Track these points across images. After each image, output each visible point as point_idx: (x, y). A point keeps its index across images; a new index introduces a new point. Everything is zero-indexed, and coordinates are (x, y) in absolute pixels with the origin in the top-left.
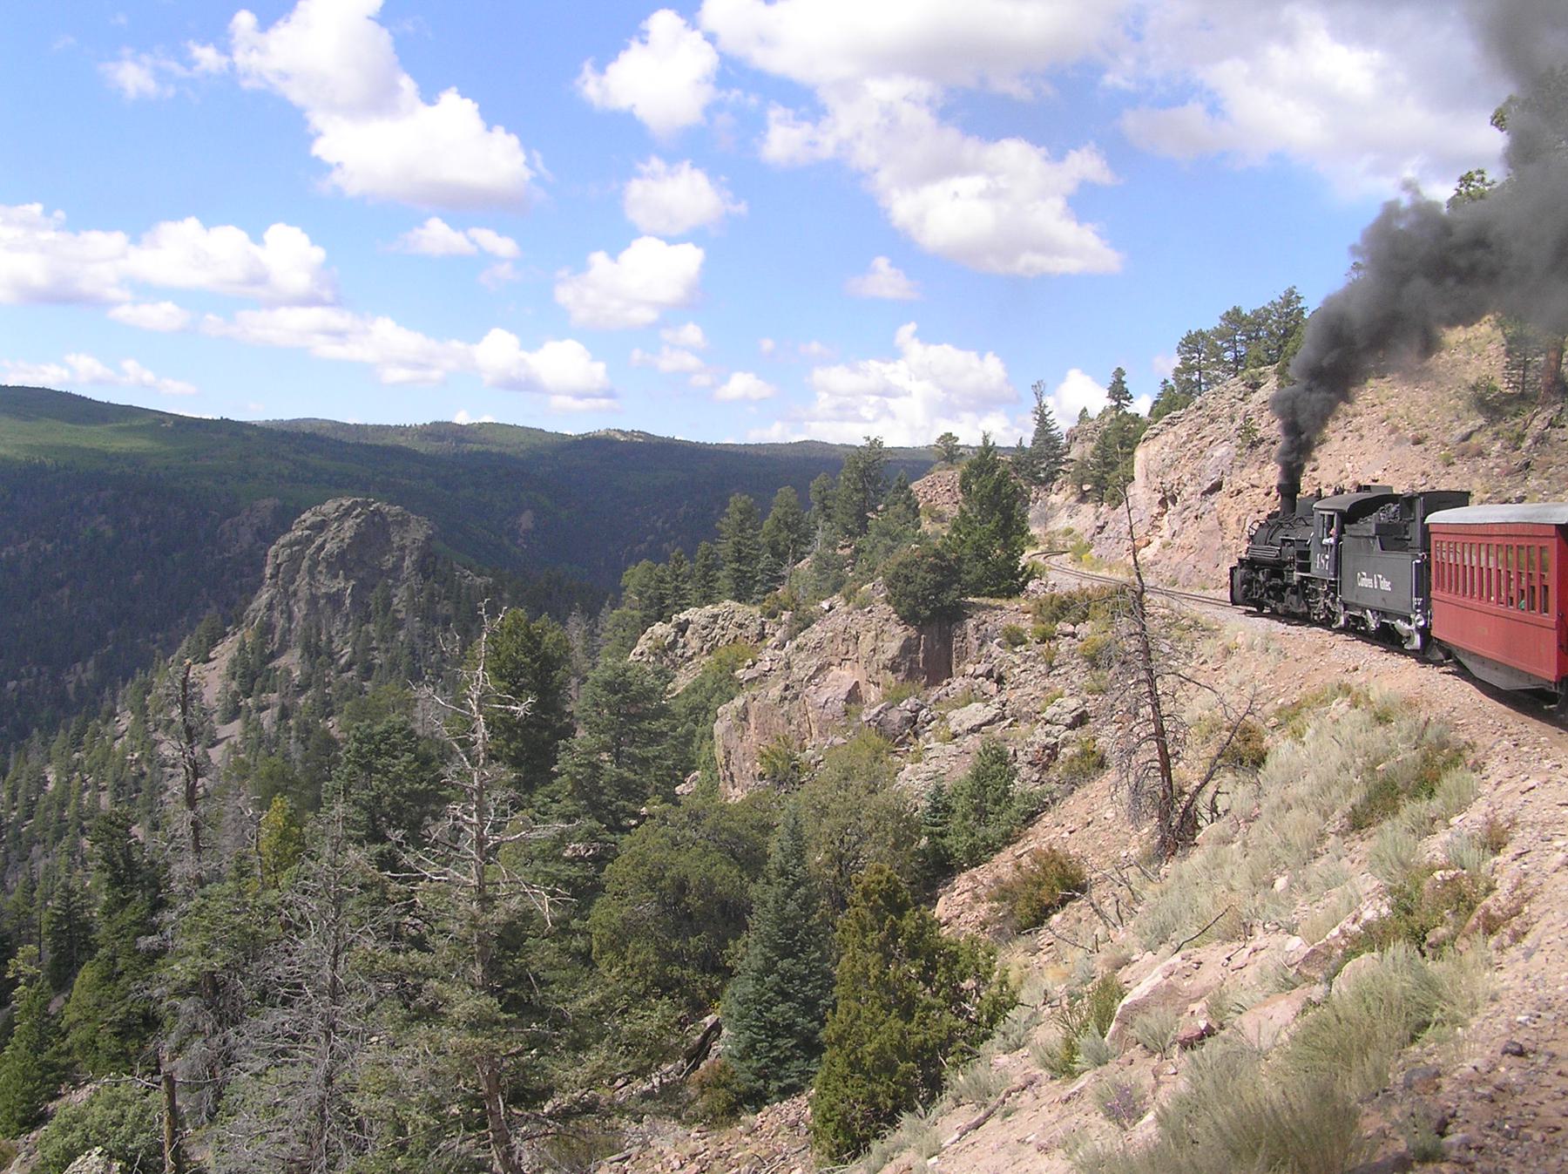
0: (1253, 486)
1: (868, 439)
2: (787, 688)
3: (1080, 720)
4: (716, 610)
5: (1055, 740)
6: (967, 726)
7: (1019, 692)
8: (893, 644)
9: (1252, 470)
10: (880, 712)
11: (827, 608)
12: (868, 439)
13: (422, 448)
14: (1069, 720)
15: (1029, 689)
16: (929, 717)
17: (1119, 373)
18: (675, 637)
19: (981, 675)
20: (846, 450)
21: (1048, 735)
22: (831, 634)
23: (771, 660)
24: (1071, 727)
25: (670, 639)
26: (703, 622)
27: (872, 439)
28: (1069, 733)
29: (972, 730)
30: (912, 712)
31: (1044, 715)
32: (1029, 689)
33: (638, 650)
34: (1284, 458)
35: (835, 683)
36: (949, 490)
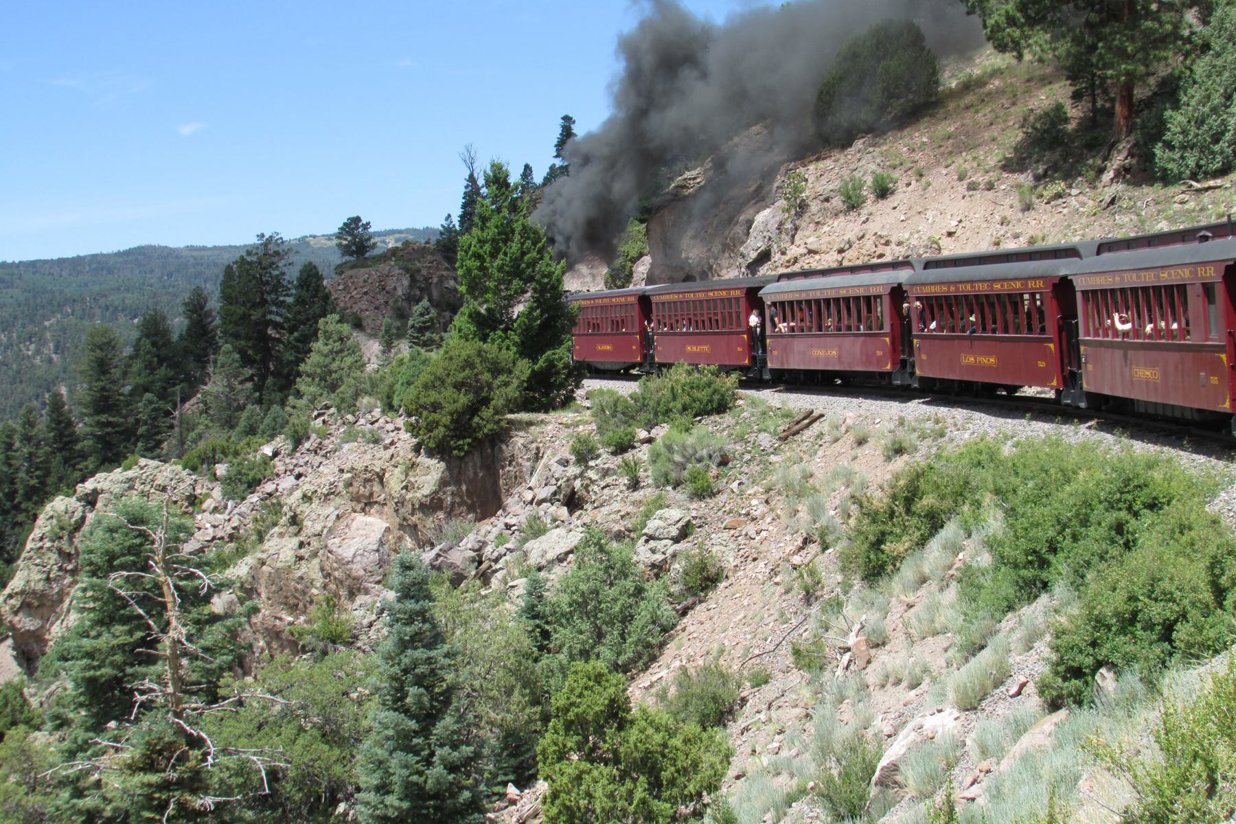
0: (811, 252)
1: (263, 235)
2: (301, 545)
3: (684, 533)
4: (130, 474)
5: (663, 557)
6: (551, 555)
7: (605, 510)
8: (429, 477)
9: (807, 233)
10: (438, 555)
11: (270, 454)
12: (263, 235)
13: (184, 253)
14: (674, 532)
15: (616, 506)
16: (496, 554)
17: (567, 119)
18: (84, 512)
19: (544, 501)
20: (195, 254)
21: (653, 551)
22: (349, 475)
23: (214, 527)
24: (676, 540)
25: (78, 515)
26: (117, 489)
27: (267, 236)
28: (677, 547)
29: (561, 559)
30: (474, 551)
31: (645, 531)
32: (616, 506)
33: (37, 533)
34: (292, 274)
35: (362, 532)
36: (366, 293)
